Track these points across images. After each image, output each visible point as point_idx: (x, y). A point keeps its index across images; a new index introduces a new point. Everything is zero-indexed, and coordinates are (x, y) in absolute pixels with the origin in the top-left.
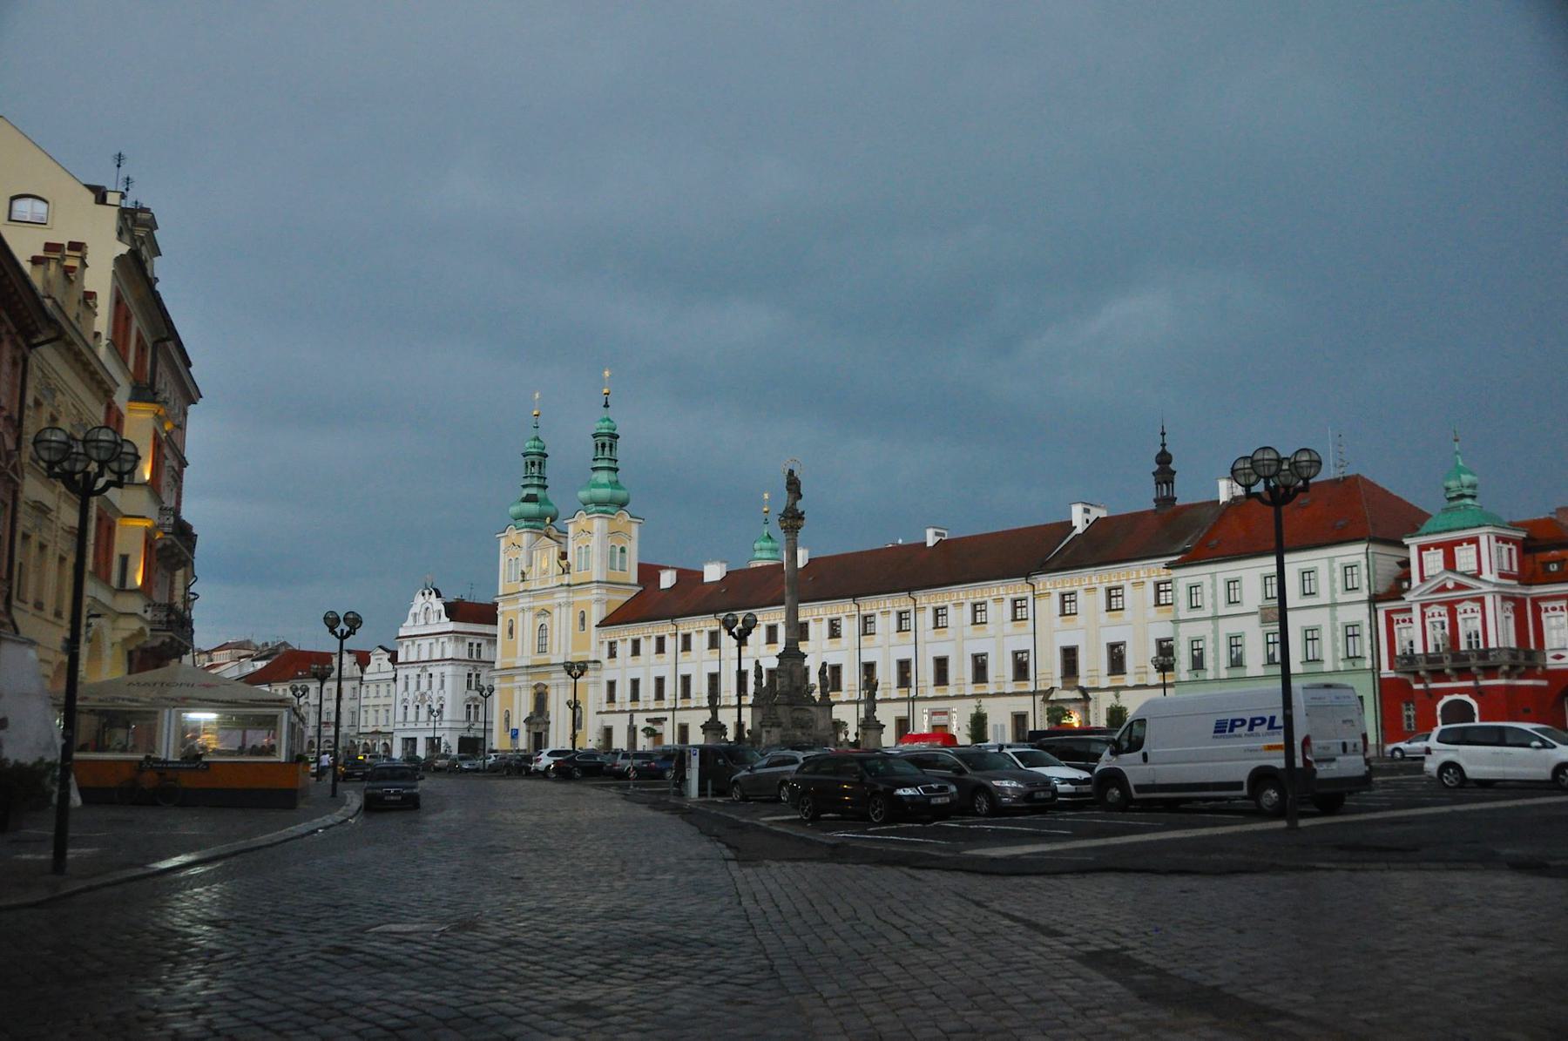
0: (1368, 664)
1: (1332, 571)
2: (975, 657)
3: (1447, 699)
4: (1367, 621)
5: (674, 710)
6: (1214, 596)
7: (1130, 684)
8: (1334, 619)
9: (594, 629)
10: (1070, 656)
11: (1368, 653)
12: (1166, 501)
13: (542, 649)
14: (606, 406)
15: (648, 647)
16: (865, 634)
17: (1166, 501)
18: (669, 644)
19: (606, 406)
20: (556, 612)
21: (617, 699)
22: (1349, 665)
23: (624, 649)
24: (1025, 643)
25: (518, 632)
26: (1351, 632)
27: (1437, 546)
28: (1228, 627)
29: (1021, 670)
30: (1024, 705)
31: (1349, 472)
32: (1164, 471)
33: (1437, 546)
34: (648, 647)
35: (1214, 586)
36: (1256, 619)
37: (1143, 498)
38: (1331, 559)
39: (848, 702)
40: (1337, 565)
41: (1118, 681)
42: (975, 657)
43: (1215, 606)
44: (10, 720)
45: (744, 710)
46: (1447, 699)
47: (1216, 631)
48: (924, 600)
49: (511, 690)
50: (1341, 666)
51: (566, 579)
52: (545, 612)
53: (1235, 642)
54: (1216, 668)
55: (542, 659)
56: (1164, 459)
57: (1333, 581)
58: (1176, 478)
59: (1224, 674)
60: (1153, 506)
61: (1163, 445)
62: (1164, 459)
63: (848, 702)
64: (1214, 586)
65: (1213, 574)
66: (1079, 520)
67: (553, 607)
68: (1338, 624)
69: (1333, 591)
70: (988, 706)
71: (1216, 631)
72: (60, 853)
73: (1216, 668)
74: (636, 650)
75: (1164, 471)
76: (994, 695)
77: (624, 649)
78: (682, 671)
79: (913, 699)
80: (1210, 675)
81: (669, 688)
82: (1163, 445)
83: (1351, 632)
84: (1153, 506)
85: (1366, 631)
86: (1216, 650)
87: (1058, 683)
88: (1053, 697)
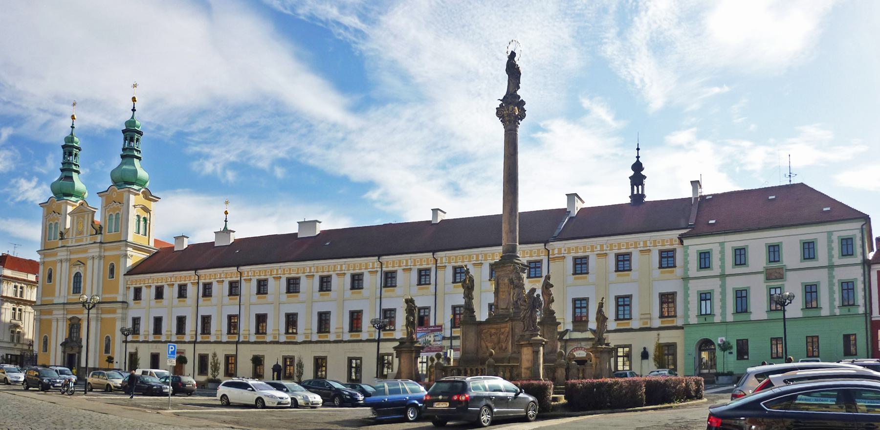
0: (861, 310)
1: (830, 242)
2: (320, 314)
4: (861, 279)
5: (195, 342)
6: (722, 259)
7: (364, 339)
8: (831, 277)
9: (121, 277)
10: (580, 304)
12: (637, 198)
13: (77, 289)
15: (170, 293)
16: (386, 286)
17: (637, 198)
18: (191, 291)
20: (89, 263)
21: (164, 331)
22: (702, 320)
23: (148, 294)
25: (57, 276)
26: (847, 288)
31: (795, 181)
32: (638, 178)
34: (170, 293)
36: (762, 277)
38: (830, 233)
39: (368, 341)
40: (835, 238)
41: (355, 336)
42: (320, 314)
43: (722, 267)
45: (382, 337)
47: (723, 287)
49: (50, 321)
51: (99, 238)
52: (81, 263)
53: (741, 296)
54: (723, 314)
55: (75, 298)
56: (638, 167)
57: (830, 249)
58: (646, 182)
59: (730, 318)
60: (628, 201)
61: (638, 157)
62: (638, 167)
63: (368, 341)
64: (722, 252)
67: (87, 258)
68: (835, 281)
69: (831, 256)
70: (188, 351)
71: (723, 287)
74: (159, 294)
76: (271, 343)
77: (148, 294)
78: (203, 312)
79: (237, 343)
80: (718, 319)
81: (190, 326)
82: (638, 157)
83: (847, 288)
84: (628, 201)
85: (860, 286)
86: (686, 302)
87: (570, 327)
88: (566, 337)
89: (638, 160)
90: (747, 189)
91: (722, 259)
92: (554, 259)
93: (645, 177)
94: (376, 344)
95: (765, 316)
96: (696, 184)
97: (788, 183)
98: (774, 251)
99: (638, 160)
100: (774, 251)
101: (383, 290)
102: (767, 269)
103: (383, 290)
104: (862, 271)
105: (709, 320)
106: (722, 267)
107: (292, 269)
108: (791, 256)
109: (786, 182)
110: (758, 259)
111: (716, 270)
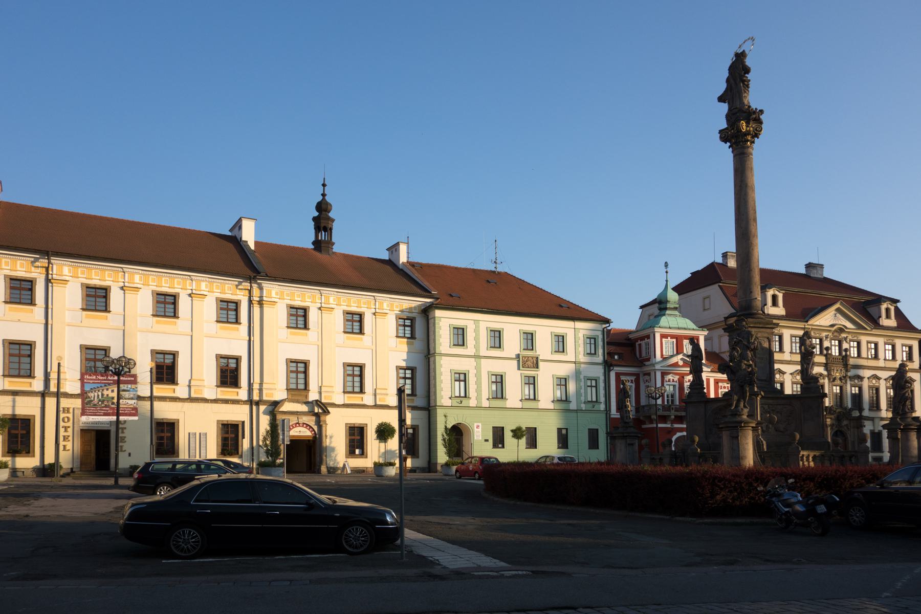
3: (679, 434)
4: (602, 378)
6: (477, 339)
10: (299, 369)
11: (602, 399)
14: (666, 265)
19: (666, 265)
22: (589, 406)
24: (34, 334)
27: (672, 337)
28: (490, 366)
29: (229, 375)
30: (239, 414)
31: (501, 269)
32: (322, 220)
33: (672, 337)
35: (477, 331)
37: (303, 237)
41: (355, 399)
43: (477, 347)
44: (747, 52)
46: (679, 434)
47: (478, 368)
48: (66, 270)
50: (583, 407)
53: (499, 380)
54: (479, 398)
56: (323, 207)
58: (335, 226)
59: (485, 403)
61: (324, 195)
62: (323, 207)
64: (477, 331)
65: (476, 322)
66: (249, 234)
71: (478, 368)
72: (118, 419)
73: (479, 398)
75: (322, 220)
80: (473, 402)
82: (324, 195)
89: (324, 199)
90: (445, 264)
91: (477, 339)
92: (418, 328)
93: (333, 220)
94: (38, 400)
95: (519, 405)
96: (394, 249)
97: (493, 269)
98: (529, 338)
99: (324, 199)
100: (529, 338)
101: (155, 386)
102: (518, 356)
103: (155, 386)
104: (602, 371)
105: (465, 402)
106: (477, 347)
107: (61, 438)
108: (544, 347)
109: (491, 267)
110: (512, 344)
111: (470, 350)
